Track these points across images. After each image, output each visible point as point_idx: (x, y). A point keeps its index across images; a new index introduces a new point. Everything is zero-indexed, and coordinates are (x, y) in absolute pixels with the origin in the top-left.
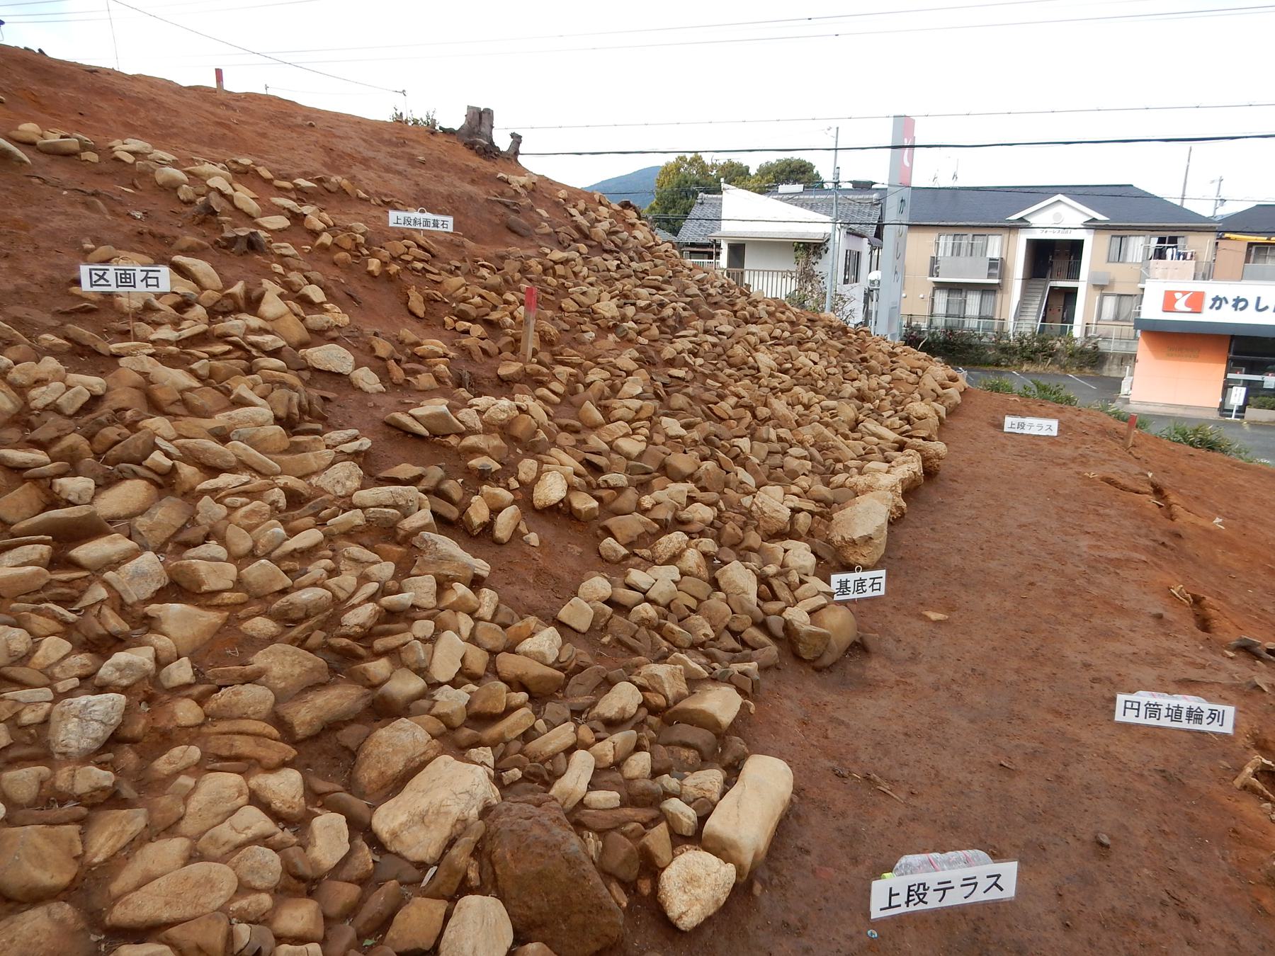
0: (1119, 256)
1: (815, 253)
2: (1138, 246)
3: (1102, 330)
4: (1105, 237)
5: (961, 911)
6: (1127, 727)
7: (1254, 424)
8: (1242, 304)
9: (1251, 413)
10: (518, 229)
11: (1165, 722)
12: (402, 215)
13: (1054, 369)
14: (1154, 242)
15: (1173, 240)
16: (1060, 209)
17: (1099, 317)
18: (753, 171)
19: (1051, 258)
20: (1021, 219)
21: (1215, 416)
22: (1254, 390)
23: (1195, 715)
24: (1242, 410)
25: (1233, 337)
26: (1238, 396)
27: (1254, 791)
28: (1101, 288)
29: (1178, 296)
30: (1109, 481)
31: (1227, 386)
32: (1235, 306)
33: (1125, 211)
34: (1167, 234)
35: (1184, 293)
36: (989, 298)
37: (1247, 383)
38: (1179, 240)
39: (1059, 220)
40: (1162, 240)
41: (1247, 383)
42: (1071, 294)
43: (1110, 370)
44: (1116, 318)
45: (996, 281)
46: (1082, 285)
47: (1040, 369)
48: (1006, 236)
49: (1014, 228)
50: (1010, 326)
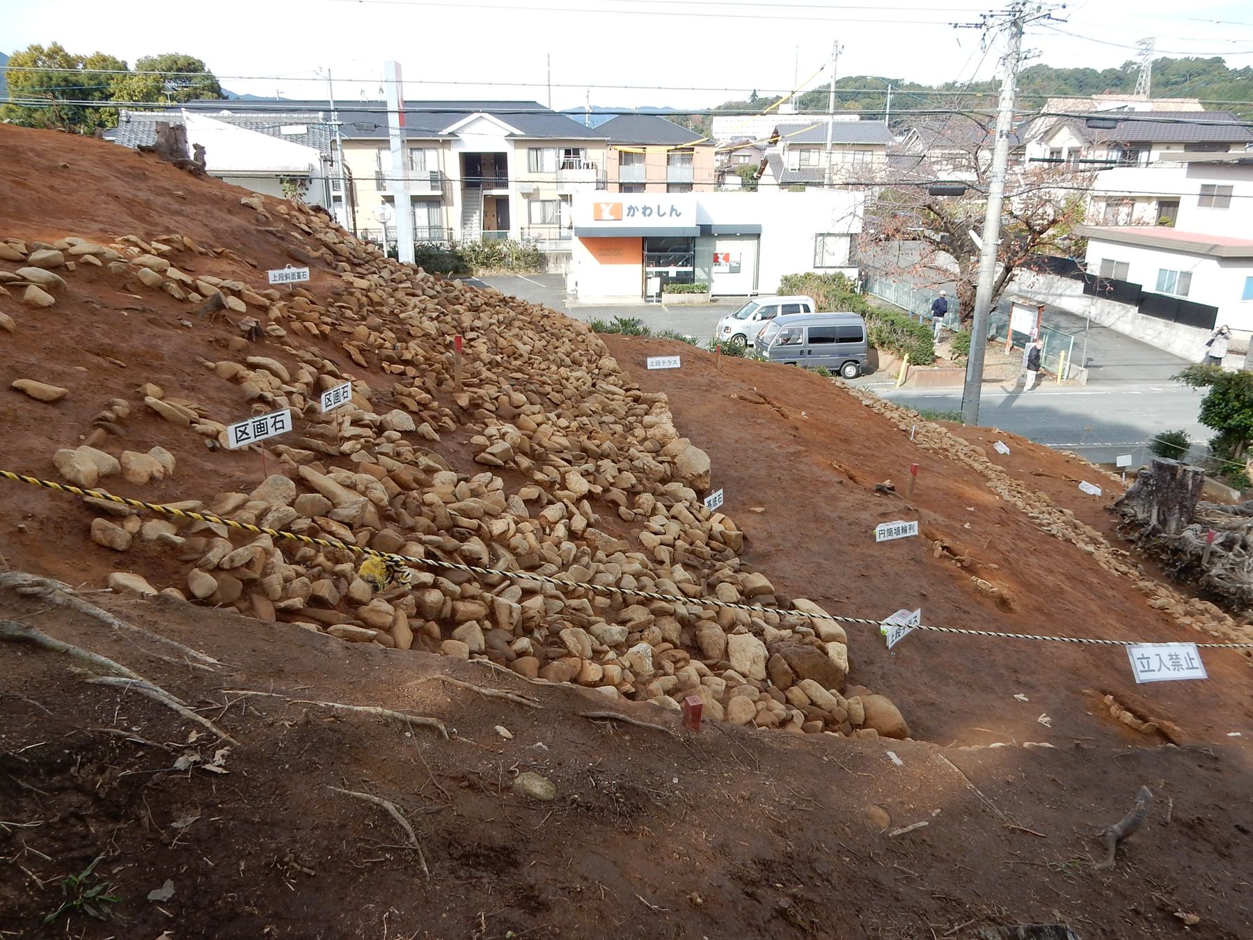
0: (536, 167)
1: (302, 184)
2: (551, 157)
3: (534, 233)
4: (523, 152)
5: (909, 635)
6: (881, 543)
7: (670, 306)
8: (648, 212)
9: (666, 297)
10: (300, 258)
11: (895, 537)
12: (277, 272)
13: (504, 272)
14: (562, 152)
15: (576, 152)
16: (482, 123)
17: (530, 222)
18: (132, 67)
19: (483, 170)
20: (452, 134)
21: (640, 301)
22: (665, 280)
23: (904, 530)
24: (659, 295)
25: (644, 239)
26: (654, 285)
27: (946, 557)
28: (530, 197)
29: (603, 206)
30: (741, 398)
31: (646, 278)
32: (644, 213)
33: (538, 124)
34: (571, 146)
35: (607, 204)
36: (434, 211)
37: (659, 274)
38: (582, 153)
39: (485, 136)
40: (568, 152)
41: (659, 274)
42: (502, 203)
43: (552, 269)
44: (544, 222)
45: (439, 193)
46: (513, 192)
47: (494, 273)
48: (441, 151)
49: (446, 143)
50: (457, 236)
